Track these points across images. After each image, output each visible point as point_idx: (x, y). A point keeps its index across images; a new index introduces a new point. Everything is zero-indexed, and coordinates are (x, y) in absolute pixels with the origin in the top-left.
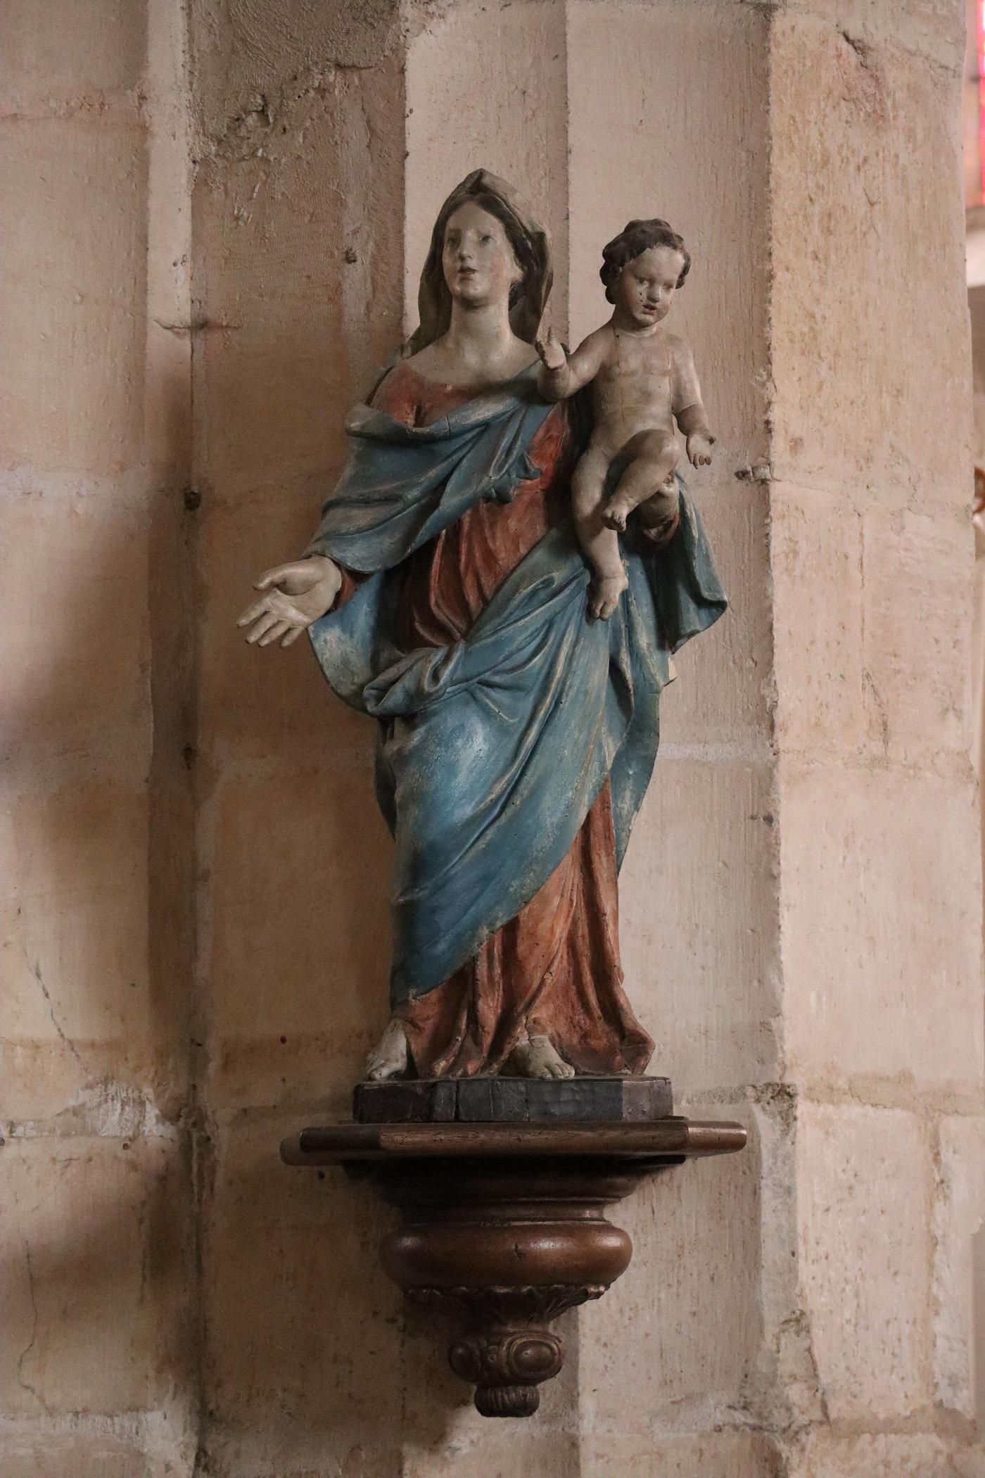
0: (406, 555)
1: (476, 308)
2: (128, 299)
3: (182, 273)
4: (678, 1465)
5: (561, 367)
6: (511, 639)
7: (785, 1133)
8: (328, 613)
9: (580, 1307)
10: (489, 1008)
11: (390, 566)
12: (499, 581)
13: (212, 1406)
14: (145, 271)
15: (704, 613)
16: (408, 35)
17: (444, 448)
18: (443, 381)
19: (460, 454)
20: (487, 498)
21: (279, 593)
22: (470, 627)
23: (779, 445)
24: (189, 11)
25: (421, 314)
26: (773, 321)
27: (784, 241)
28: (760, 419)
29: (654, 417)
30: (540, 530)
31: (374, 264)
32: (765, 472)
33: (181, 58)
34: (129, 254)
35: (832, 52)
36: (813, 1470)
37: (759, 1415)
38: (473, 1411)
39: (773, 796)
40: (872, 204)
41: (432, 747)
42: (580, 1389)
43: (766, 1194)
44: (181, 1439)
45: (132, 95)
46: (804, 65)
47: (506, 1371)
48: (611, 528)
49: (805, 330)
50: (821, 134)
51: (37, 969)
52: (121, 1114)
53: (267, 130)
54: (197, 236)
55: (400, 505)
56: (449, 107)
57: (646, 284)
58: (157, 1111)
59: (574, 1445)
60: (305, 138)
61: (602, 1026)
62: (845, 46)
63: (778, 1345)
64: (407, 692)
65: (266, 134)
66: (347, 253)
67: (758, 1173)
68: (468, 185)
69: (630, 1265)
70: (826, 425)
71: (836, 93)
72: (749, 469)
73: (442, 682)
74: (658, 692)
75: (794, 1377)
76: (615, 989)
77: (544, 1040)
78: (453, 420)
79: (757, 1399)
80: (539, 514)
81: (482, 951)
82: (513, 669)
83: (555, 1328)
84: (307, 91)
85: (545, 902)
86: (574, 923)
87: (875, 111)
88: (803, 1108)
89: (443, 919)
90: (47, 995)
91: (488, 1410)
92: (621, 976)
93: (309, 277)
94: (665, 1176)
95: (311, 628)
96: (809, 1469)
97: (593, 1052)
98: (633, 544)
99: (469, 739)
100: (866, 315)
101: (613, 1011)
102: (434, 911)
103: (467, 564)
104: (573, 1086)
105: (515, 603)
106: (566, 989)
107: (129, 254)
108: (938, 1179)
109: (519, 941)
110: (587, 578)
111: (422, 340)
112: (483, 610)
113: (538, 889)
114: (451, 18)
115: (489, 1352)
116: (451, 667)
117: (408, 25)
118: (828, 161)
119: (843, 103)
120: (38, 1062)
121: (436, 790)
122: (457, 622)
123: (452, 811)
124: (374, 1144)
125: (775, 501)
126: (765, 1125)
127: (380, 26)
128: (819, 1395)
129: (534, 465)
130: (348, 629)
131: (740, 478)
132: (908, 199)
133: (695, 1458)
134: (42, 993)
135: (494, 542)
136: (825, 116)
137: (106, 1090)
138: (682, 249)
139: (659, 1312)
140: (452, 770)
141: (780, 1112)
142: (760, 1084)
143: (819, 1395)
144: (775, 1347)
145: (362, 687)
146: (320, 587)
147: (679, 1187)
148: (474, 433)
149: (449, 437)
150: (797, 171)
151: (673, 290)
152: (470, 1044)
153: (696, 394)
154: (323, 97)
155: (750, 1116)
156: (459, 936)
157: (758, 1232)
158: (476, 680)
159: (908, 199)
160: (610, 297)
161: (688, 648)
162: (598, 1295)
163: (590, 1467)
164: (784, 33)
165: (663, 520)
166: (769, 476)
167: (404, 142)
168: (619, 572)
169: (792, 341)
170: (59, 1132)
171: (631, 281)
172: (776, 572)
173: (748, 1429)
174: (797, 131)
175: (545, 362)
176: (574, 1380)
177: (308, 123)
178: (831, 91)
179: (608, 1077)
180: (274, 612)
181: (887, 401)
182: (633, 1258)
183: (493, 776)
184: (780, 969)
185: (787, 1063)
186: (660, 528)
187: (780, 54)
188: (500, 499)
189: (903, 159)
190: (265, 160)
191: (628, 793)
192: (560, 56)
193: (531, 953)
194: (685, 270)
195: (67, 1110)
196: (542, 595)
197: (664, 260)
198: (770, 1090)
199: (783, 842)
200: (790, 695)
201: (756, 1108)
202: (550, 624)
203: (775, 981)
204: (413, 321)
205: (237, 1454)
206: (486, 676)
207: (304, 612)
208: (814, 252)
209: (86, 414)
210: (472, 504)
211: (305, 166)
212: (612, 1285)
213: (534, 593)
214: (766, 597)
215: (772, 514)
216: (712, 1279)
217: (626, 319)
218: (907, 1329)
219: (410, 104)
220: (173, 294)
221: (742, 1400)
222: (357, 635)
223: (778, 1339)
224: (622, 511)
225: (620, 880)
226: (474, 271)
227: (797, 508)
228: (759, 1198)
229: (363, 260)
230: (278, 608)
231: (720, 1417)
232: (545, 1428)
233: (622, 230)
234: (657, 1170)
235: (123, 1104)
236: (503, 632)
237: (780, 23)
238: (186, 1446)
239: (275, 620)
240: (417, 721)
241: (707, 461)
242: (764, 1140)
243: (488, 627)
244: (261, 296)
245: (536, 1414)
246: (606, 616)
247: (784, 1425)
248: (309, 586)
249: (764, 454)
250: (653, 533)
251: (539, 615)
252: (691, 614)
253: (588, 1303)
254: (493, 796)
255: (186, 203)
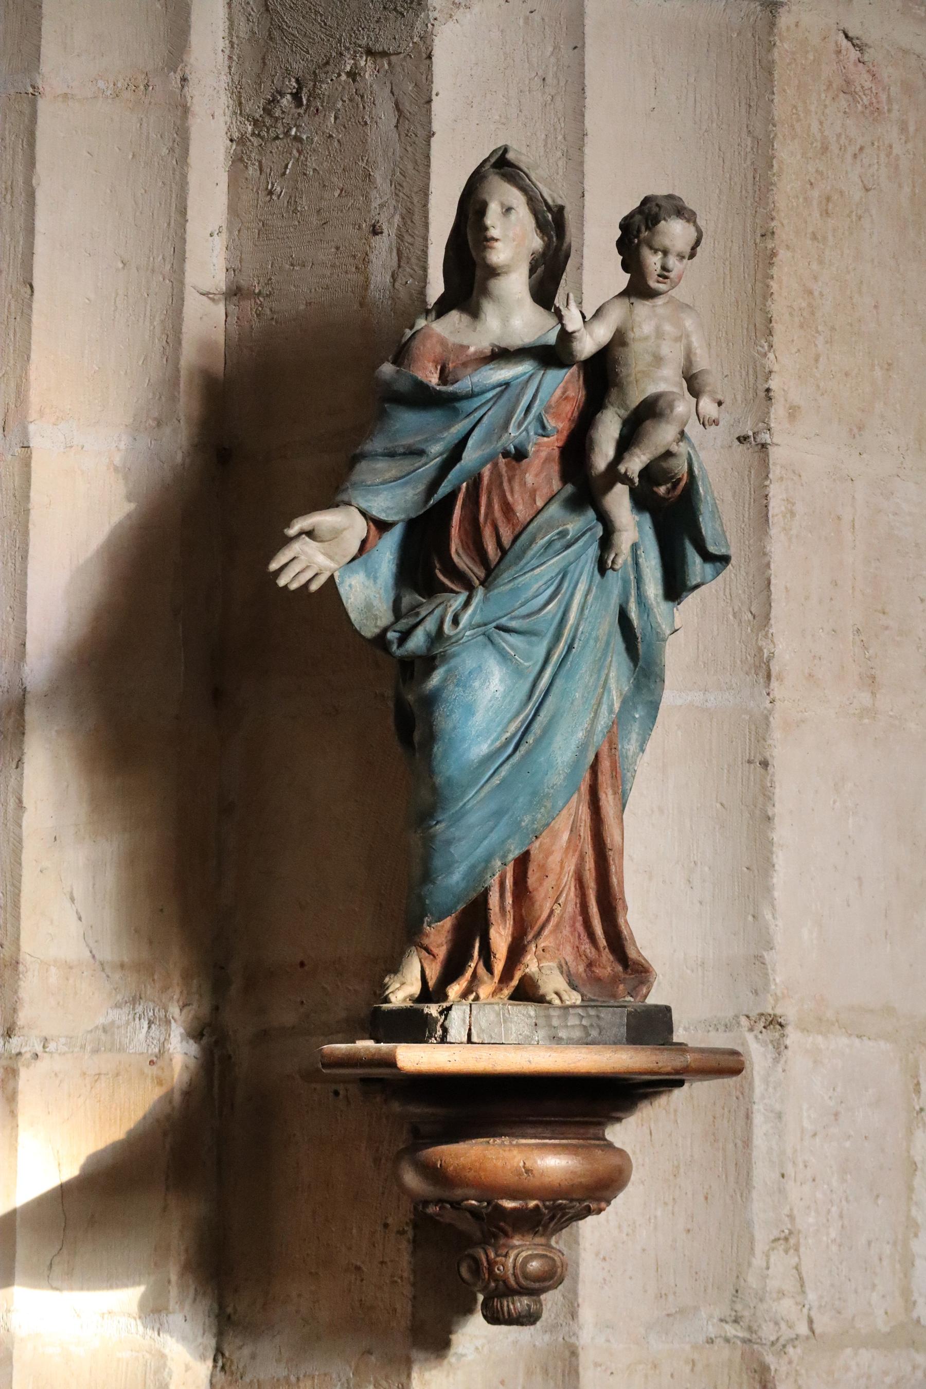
0: (428, 506)
1: (498, 275)
2: (168, 267)
3: (219, 243)
4: (672, 1376)
5: (579, 331)
6: (527, 586)
7: (776, 1060)
8: (353, 559)
9: (581, 1223)
10: (500, 938)
11: (413, 516)
12: (516, 532)
13: (229, 1310)
14: (184, 240)
15: (709, 568)
16: (436, 23)
17: (466, 406)
18: (465, 343)
19: (477, 415)
20: (506, 454)
21: (307, 539)
22: (488, 575)
23: (778, 412)
24: (229, 5)
25: (445, 282)
26: (775, 297)
27: (785, 222)
28: (762, 387)
29: (665, 380)
30: (556, 484)
31: (400, 237)
32: (765, 437)
33: (222, 44)
34: (169, 224)
35: (832, 47)
36: (800, 1382)
37: (750, 1329)
38: (477, 1321)
39: (770, 742)
40: (867, 190)
41: (451, 687)
42: (580, 1300)
43: (758, 1119)
44: (200, 1340)
45: (175, 78)
46: (806, 59)
47: (512, 1281)
48: (623, 483)
49: (804, 305)
50: (821, 123)
51: (71, 893)
52: (148, 1032)
53: (301, 111)
54: (233, 209)
55: (424, 460)
56: (471, 93)
57: (660, 255)
58: (182, 1030)
59: (574, 1353)
60: (336, 118)
61: (607, 956)
62: (845, 43)
63: (768, 1263)
64: (428, 635)
65: (299, 114)
66: (374, 226)
67: (751, 1097)
68: (493, 160)
69: (630, 1184)
70: (822, 394)
71: (834, 86)
72: (751, 433)
73: (461, 626)
74: (664, 640)
75: (782, 1294)
76: (621, 921)
77: (550, 965)
78: (475, 379)
79: (746, 1313)
80: (554, 469)
81: (494, 882)
82: (529, 615)
83: (557, 1243)
84: (339, 75)
85: (555, 836)
86: (582, 858)
87: (871, 104)
88: (793, 1036)
89: (457, 850)
90: (80, 919)
91: (494, 1318)
92: (625, 908)
93: (337, 248)
94: (662, 1100)
95: (336, 575)
96: (796, 1381)
97: (598, 980)
98: (642, 500)
99: (486, 680)
100: (860, 292)
101: (617, 942)
102: (449, 843)
103: (486, 515)
104: (580, 1011)
105: (530, 553)
106: (573, 919)
107: (169, 224)
108: (917, 1108)
109: (530, 872)
110: (599, 531)
111: (443, 307)
112: (501, 559)
113: (548, 825)
114: (476, 9)
115: (496, 1263)
116: (470, 611)
117: (436, 14)
118: (827, 148)
119: (842, 95)
120: (71, 981)
121: (455, 728)
122: (476, 570)
123: (469, 748)
124: (390, 1062)
125: (774, 464)
126: (757, 1053)
127: (409, 15)
128: (805, 1310)
129: (551, 423)
130: (372, 575)
131: (740, 442)
132: (900, 186)
133: (687, 1369)
134: (75, 917)
135: (512, 495)
136: (826, 106)
137: (134, 1009)
138: (695, 222)
139: (655, 1228)
140: (470, 710)
141: (772, 1041)
142: (754, 1014)
143: (805, 1310)
144: (765, 1264)
145: (385, 630)
146: (347, 534)
147: (675, 1111)
148: (498, 389)
149: (471, 395)
150: (799, 157)
151: (685, 261)
152: (482, 970)
153: (702, 362)
154: (354, 81)
155: (744, 1044)
156: (473, 867)
157: (750, 1154)
158: (494, 624)
159: (900, 186)
160: (626, 266)
161: (691, 601)
162: (599, 1211)
163: (589, 1376)
164: (788, 28)
165: (672, 477)
166: (769, 441)
167: (430, 123)
168: (631, 526)
169: (791, 314)
170: (88, 1048)
171: (646, 253)
172: (774, 531)
173: (739, 1343)
174: (799, 120)
175: (563, 325)
176: (574, 1292)
177: (339, 105)
178: (830, 84)
179: (612, 1003)
180: (303, 557)
181: (878, 373)
182: (633, 1178)
183: (509, 715)
184: (773, 906)
185: (779, 994)
186: (669, 485)
187: (784, 48)
188: (519, 455)
189: (897, 150)
190: (297, 139)
191: (634, 736)
192: (578, 47)
193: (541, 884)
194: (698, 242)
195: (97, 1027)
196: (558, 545)
197: (675, 232)
198: (763, 1019)
199: (777, 785)
200: (785, 647)
201: (750, 1037)
202: (564, 574)
203: (769, 917)
204: (436, 288)
205: (253, 1357)
206: (503, 621)
207: (331, 558)
208: (813, 233)
209: (126, 373)
210: (491, 459)
211: (336, 143)
212: (613, 1202)
213: (550, 543)
214: (765, 554)
215: (771, 476)
216: (706, 1198)
217: (638, 289)
218: (887, 1249)
219: (436, 87)
220: (209, 262)
221: (733, 1314)
222: (380, 581)
223: (768, 1256)
224: (634, 464)
225: (624, 816)
226: (497, 240)
227: (794, 472)
228: (751, 1123)
229: (389, 231)
230: (305, 553)
231: (712, 1331)
232: (547, 1337)
233: (638, 204)
234: (657, 1094)
235: (150, 1023)
236: (520, 579)
237: (785, 20)
238: (205, 1348)
239: (304, 566)
240: (437, 662)
241: (716, 422)
242: (757, 1068)
243: (505, 575)
244: (292, 265)
245: (538, 1323)
246: (616, 567)
247: (773, 1338)
248: (336, 534)
249: (764, 419)
250: (662, 490)
251: (554, 564)
252: (696, 566)
253: (589, 1218)
254: (508, 735)
255: (223, 178)
